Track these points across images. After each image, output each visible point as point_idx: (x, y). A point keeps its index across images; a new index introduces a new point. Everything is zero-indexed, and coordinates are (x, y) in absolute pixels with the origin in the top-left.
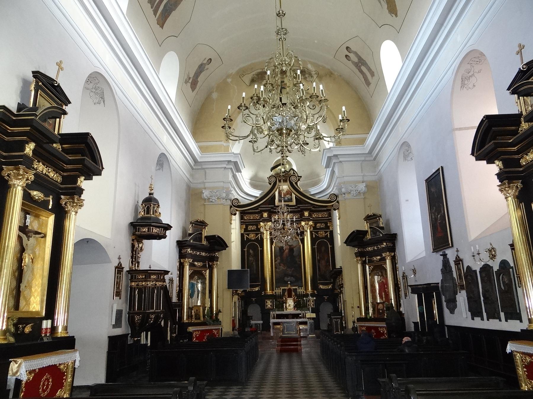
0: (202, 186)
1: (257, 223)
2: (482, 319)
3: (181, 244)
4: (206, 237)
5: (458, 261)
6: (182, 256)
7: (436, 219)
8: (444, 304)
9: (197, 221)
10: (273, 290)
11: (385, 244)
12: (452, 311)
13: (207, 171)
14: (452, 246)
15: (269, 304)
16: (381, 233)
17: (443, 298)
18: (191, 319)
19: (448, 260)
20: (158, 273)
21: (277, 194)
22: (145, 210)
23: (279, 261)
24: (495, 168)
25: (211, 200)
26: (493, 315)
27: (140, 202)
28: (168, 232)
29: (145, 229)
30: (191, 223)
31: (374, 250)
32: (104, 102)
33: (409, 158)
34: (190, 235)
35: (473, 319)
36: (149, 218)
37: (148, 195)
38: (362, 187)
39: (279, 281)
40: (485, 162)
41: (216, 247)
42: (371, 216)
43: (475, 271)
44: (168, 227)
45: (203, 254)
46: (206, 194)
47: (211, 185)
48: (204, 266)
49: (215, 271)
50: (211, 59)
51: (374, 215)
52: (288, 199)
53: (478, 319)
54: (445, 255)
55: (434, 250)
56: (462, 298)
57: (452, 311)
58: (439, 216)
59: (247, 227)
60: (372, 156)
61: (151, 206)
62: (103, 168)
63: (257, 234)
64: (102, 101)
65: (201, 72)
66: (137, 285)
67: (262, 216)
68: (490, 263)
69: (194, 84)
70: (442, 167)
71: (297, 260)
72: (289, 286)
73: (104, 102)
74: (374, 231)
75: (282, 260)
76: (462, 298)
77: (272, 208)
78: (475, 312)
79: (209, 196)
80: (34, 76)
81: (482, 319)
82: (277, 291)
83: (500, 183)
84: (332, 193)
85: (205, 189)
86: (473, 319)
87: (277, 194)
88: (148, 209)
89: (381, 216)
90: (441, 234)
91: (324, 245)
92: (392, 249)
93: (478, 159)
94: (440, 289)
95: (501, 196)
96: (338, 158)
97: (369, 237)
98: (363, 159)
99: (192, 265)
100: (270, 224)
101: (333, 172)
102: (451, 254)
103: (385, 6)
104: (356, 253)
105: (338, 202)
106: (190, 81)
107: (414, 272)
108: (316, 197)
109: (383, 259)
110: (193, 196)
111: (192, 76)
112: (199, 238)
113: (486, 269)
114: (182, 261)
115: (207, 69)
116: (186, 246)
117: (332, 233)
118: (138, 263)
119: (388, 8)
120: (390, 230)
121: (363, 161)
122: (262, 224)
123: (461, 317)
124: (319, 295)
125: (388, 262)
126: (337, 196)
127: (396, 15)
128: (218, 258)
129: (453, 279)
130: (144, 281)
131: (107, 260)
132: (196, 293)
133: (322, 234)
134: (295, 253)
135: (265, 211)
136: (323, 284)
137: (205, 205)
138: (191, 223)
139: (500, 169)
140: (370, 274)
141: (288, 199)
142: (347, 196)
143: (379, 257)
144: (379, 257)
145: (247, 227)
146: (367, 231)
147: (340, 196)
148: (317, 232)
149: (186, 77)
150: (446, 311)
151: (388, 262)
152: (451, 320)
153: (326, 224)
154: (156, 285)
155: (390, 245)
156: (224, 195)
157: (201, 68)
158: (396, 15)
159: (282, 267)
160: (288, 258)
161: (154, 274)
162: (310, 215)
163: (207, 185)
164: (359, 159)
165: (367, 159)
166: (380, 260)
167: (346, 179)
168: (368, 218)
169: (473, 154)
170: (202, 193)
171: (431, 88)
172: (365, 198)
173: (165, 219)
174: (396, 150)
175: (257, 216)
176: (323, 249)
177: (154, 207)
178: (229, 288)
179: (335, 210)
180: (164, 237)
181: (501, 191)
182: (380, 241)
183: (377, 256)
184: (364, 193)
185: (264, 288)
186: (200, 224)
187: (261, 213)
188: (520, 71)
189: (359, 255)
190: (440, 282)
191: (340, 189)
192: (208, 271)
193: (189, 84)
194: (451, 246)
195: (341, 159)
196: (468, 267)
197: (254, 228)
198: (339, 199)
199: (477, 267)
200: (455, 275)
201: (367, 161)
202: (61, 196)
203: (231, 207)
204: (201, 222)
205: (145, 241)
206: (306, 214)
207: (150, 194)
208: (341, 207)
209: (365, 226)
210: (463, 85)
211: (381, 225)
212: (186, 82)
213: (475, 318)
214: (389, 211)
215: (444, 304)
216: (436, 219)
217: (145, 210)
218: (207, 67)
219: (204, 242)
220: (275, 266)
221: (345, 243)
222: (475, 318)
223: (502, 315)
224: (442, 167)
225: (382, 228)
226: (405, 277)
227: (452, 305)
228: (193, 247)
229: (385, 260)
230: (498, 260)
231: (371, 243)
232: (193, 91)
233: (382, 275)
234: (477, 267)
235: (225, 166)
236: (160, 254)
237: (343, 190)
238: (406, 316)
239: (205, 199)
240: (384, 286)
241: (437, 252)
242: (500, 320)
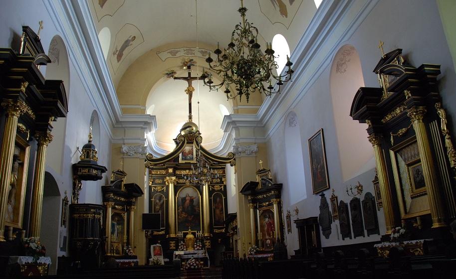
0: (121, 142)
1: (163, 177)
2: (351, 238)
3: (105, 190)
4: (125, 185)
5: (334, 198)
6: (105, 199)
7: (317, 169)
8: (321, 232)
9: (118, 171)
10: (176, 234)
11: (273, 192)
12: (327, 237)
13: (126, 129)
14: (329, 188)
15: (172, 244)
16: (271, 184)
17: (321, 228)
18: (113, 253)
19: (325, 198)
20: (96, 208)
21: (180, 155)
22: (85, 155)
23: (181, 210)
24: (366, 126)
25: (129, 154)
26: (359, 233)
27: (80, 149)
28: (104, 175)
29: (86, 170)
30: (113, 172)
31: (264, 197)
32: (58, 61)
33: (293, 125)
34: (112, 182)
35: (343, 239)
36: (90, 161)
37: (87, 142)
38: (254, 148)
39: (182, 224)
40: (358, 121)
41: (134, 194)
42: (261, 170)
43: (346, 205)
44: (103, 170)
45: (123, 199)
46: (125, 149)
47: (130, 141)
48: (123, 210)
49: (132, 213)
50: (135, 37)
51: (264, 170)
52: (190, 158)
53: (347, 239)
54: (323, 195)
55: (314, 192)
56: (336, 225)
57: (327, 237)
58: (319, 166)
59: (154, 180)
60: (262, 124)
61: (90, 151)
62: (68, 111)
63: (163, 187)
64: (57, 61)
65: (126, 46)
66: (79, 216)
67: (167, 172)
68: (358, 197)
69: (119, 57)
70: (322, 130)
71: (197, 209)
72: (190, 230)
73: (58, 61)
74: (264, 184)
75: (184, 208)
76: (336, 225)
77: (177, 165)
78: (345, 233)
79: (127, 150)
80: (24, 31)
81: (351, 238)
82: (179, 235)
83: (369, 136)
84: (229, 152)
85: (124, 144)
86: (343, 239)
87: (180, 155)
88: (88, 153)
89: (270, 171)
90: (320, 178)
91: (219, 196)
92: (279, 196)
93: (354, 119)
94: (319, 222)
95: (370, 144)
96: (236, 124)
97: (260, 187)
98: (255, 125)
99: (113, 208)
100: (174, 178)
101: (230, 135)
102: (328, 195)
103: (278, 9)
104: (249, 200)
105: (235, 159)
106: (117, 53)
107: (297, 211)
108: (219, 155)
109: (271, 205)
110: (116, 150)
111: (118, 49)
112: (119, 186)
113: (355, 202)
114: (105, 203)
115: (131, 45)
116: (109, 191)
117: (225, 186)
118: (78, 199)
119: (280, 11)
120: (276, 181)
121: (255, 127)
122: (168, 178)
123: (334, 239)
124: (214, 238)
125: (275, 206)
126: (234, 154)
127: (286, 16)
128: (134, 203)
129: (329, 212)
130: (85, 213)
131: (58, 194)
132: (116, 231)
133: (217, 187)
134: (195, 203)
135: (171, 167)
136: (218, 228)
137: (123, 158)
138: (113, 172)
139: (369, 126)
140: (260, 217)
141: (190, 158)
142: (242, 155)
143: (267, 203)
144: (267, 203)
145: (154, 180)
146: (258, 183)
147: (236, 155)
148: (213, 186)
149: (114, 49)
150: (323, 237)
151: (275, 206)
152: (326, 243)
153: (221, 179)
154: (95, 217)
155: (276, 192)
156: (141, 150)
157: (126, 44)
158: (286, 16)
159: (183, 215)
160: (189, 210)
161: (94, 208)
162: (174, 171)
163: (126, 141)
164: (252, 125)
165: (259, 125)
166: (269, 205)
167: (241, 141)
168: (260, 172)
169: (351, 115)
170: (121, 148)
171: (322, 70)
172: (256, 157)
173: (100, 163)
174: (283, 118)
175: (164, 172)
176: (218, 199)
177: (93, 153)
178: (144, 228)
179: (232, 166)
180: (100, 178)
181: (370, 141)
182: (269, 190)
183: (266, 202)
184: (256, 153)
185: (168, 231)
186: (122, 173)
187: (167, 169)
188: (382, 59)
189: (254, 201)
190: (318, 216)
191: (237, 149)
192: (126, 214)
193: (116, 56)
194: (328, 187)
195: (238, 125)
196: (341, 202)
197: (160, 181)
198: (236, 156)
199: (347, 200)
200: (330, 209)
201: (258, 127)
202: (38, 130)
203: (146, 161)
204: (121, 172)
205: (83, 182)
206: (171, 171)
207: (90, 141)
208: (236, 165)
209: (258, 179)
210: (338, 70)
211: (270, 178)
212: (114, 54)
213: (345, 239)
214: (276, 166)
215: (321, 232)
216: (317, 169)
217: (85, 155)
218: (131, 43)
219: (123, 189)
220: (178, 214)
221: (241, 192)
222: (345, 239)
223: (365, 231)
224: (322, 130)
225: (271, 180)
226: (288, 217)
227: (328, 232)
228: (116, 194)
229: (273, 205)
230: (364, 193)
231: (261, 193)
232: (118, 61)
233: (269, 218)
234: (347, 200)
235: (141, 126)
236: (91, 193)
237: (240, 149)
238: (288, 248)
239: (124, 153)
240: (271, 225)
241: (317, 194)
242: (364, 237)
